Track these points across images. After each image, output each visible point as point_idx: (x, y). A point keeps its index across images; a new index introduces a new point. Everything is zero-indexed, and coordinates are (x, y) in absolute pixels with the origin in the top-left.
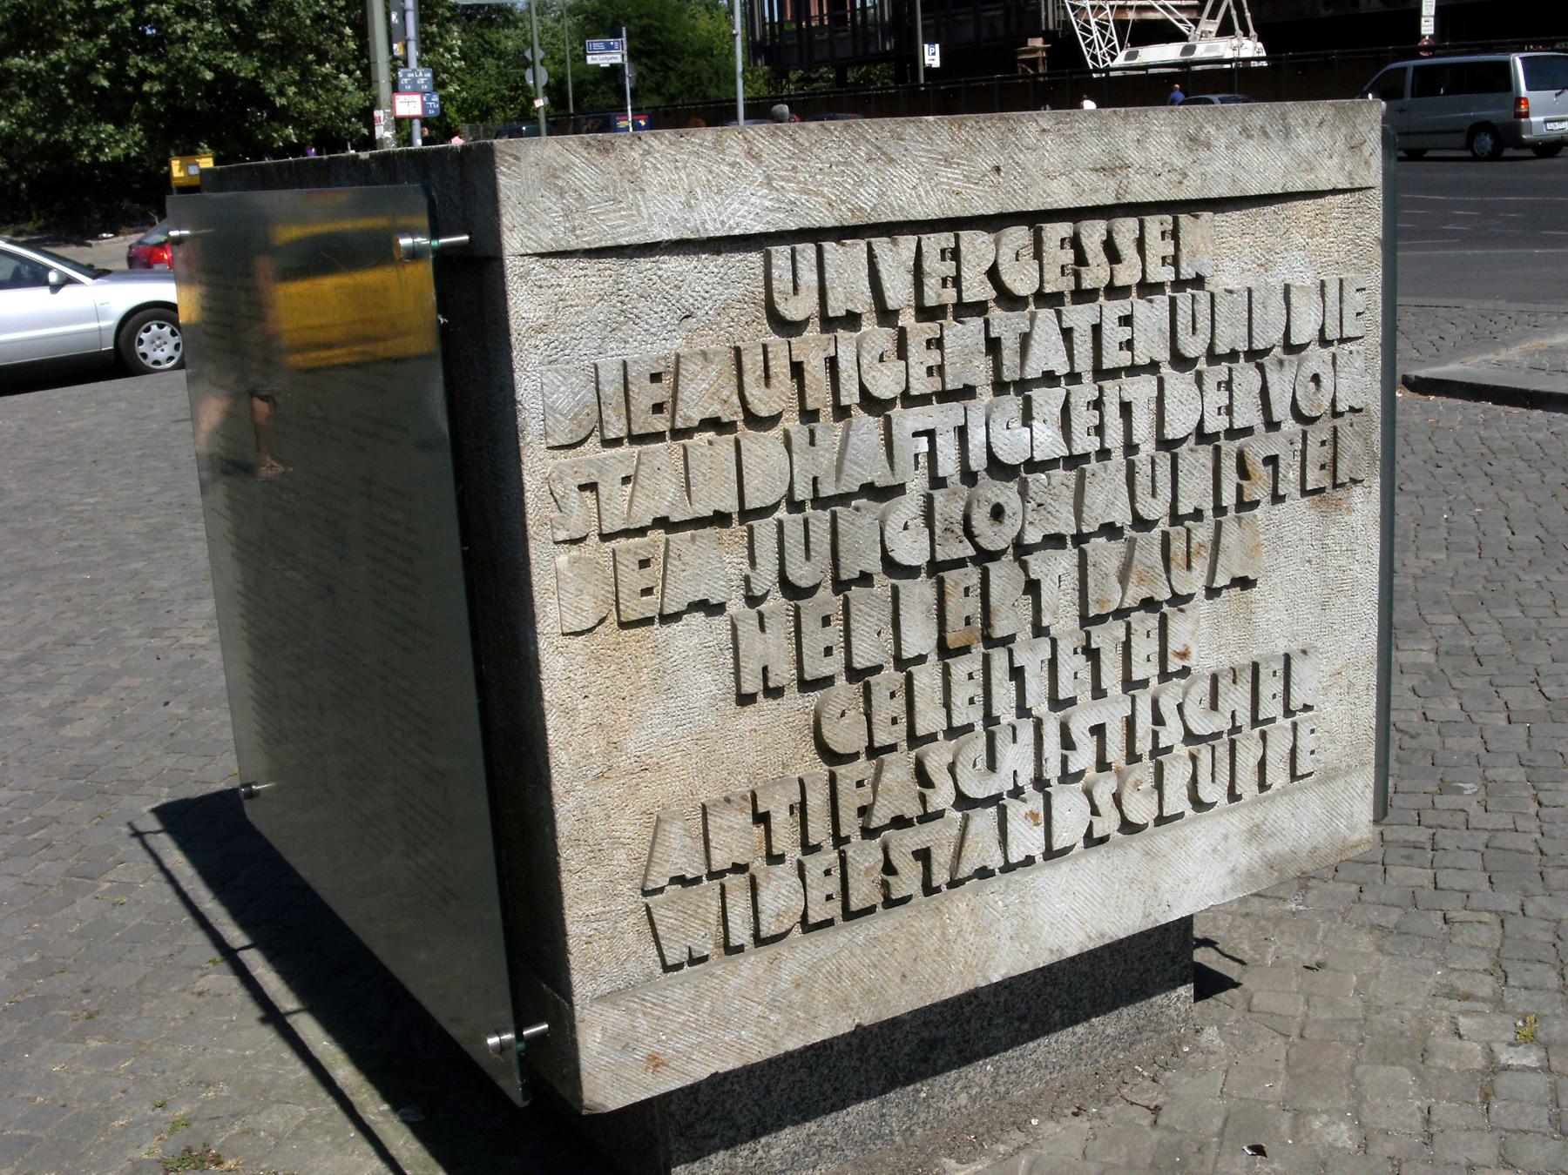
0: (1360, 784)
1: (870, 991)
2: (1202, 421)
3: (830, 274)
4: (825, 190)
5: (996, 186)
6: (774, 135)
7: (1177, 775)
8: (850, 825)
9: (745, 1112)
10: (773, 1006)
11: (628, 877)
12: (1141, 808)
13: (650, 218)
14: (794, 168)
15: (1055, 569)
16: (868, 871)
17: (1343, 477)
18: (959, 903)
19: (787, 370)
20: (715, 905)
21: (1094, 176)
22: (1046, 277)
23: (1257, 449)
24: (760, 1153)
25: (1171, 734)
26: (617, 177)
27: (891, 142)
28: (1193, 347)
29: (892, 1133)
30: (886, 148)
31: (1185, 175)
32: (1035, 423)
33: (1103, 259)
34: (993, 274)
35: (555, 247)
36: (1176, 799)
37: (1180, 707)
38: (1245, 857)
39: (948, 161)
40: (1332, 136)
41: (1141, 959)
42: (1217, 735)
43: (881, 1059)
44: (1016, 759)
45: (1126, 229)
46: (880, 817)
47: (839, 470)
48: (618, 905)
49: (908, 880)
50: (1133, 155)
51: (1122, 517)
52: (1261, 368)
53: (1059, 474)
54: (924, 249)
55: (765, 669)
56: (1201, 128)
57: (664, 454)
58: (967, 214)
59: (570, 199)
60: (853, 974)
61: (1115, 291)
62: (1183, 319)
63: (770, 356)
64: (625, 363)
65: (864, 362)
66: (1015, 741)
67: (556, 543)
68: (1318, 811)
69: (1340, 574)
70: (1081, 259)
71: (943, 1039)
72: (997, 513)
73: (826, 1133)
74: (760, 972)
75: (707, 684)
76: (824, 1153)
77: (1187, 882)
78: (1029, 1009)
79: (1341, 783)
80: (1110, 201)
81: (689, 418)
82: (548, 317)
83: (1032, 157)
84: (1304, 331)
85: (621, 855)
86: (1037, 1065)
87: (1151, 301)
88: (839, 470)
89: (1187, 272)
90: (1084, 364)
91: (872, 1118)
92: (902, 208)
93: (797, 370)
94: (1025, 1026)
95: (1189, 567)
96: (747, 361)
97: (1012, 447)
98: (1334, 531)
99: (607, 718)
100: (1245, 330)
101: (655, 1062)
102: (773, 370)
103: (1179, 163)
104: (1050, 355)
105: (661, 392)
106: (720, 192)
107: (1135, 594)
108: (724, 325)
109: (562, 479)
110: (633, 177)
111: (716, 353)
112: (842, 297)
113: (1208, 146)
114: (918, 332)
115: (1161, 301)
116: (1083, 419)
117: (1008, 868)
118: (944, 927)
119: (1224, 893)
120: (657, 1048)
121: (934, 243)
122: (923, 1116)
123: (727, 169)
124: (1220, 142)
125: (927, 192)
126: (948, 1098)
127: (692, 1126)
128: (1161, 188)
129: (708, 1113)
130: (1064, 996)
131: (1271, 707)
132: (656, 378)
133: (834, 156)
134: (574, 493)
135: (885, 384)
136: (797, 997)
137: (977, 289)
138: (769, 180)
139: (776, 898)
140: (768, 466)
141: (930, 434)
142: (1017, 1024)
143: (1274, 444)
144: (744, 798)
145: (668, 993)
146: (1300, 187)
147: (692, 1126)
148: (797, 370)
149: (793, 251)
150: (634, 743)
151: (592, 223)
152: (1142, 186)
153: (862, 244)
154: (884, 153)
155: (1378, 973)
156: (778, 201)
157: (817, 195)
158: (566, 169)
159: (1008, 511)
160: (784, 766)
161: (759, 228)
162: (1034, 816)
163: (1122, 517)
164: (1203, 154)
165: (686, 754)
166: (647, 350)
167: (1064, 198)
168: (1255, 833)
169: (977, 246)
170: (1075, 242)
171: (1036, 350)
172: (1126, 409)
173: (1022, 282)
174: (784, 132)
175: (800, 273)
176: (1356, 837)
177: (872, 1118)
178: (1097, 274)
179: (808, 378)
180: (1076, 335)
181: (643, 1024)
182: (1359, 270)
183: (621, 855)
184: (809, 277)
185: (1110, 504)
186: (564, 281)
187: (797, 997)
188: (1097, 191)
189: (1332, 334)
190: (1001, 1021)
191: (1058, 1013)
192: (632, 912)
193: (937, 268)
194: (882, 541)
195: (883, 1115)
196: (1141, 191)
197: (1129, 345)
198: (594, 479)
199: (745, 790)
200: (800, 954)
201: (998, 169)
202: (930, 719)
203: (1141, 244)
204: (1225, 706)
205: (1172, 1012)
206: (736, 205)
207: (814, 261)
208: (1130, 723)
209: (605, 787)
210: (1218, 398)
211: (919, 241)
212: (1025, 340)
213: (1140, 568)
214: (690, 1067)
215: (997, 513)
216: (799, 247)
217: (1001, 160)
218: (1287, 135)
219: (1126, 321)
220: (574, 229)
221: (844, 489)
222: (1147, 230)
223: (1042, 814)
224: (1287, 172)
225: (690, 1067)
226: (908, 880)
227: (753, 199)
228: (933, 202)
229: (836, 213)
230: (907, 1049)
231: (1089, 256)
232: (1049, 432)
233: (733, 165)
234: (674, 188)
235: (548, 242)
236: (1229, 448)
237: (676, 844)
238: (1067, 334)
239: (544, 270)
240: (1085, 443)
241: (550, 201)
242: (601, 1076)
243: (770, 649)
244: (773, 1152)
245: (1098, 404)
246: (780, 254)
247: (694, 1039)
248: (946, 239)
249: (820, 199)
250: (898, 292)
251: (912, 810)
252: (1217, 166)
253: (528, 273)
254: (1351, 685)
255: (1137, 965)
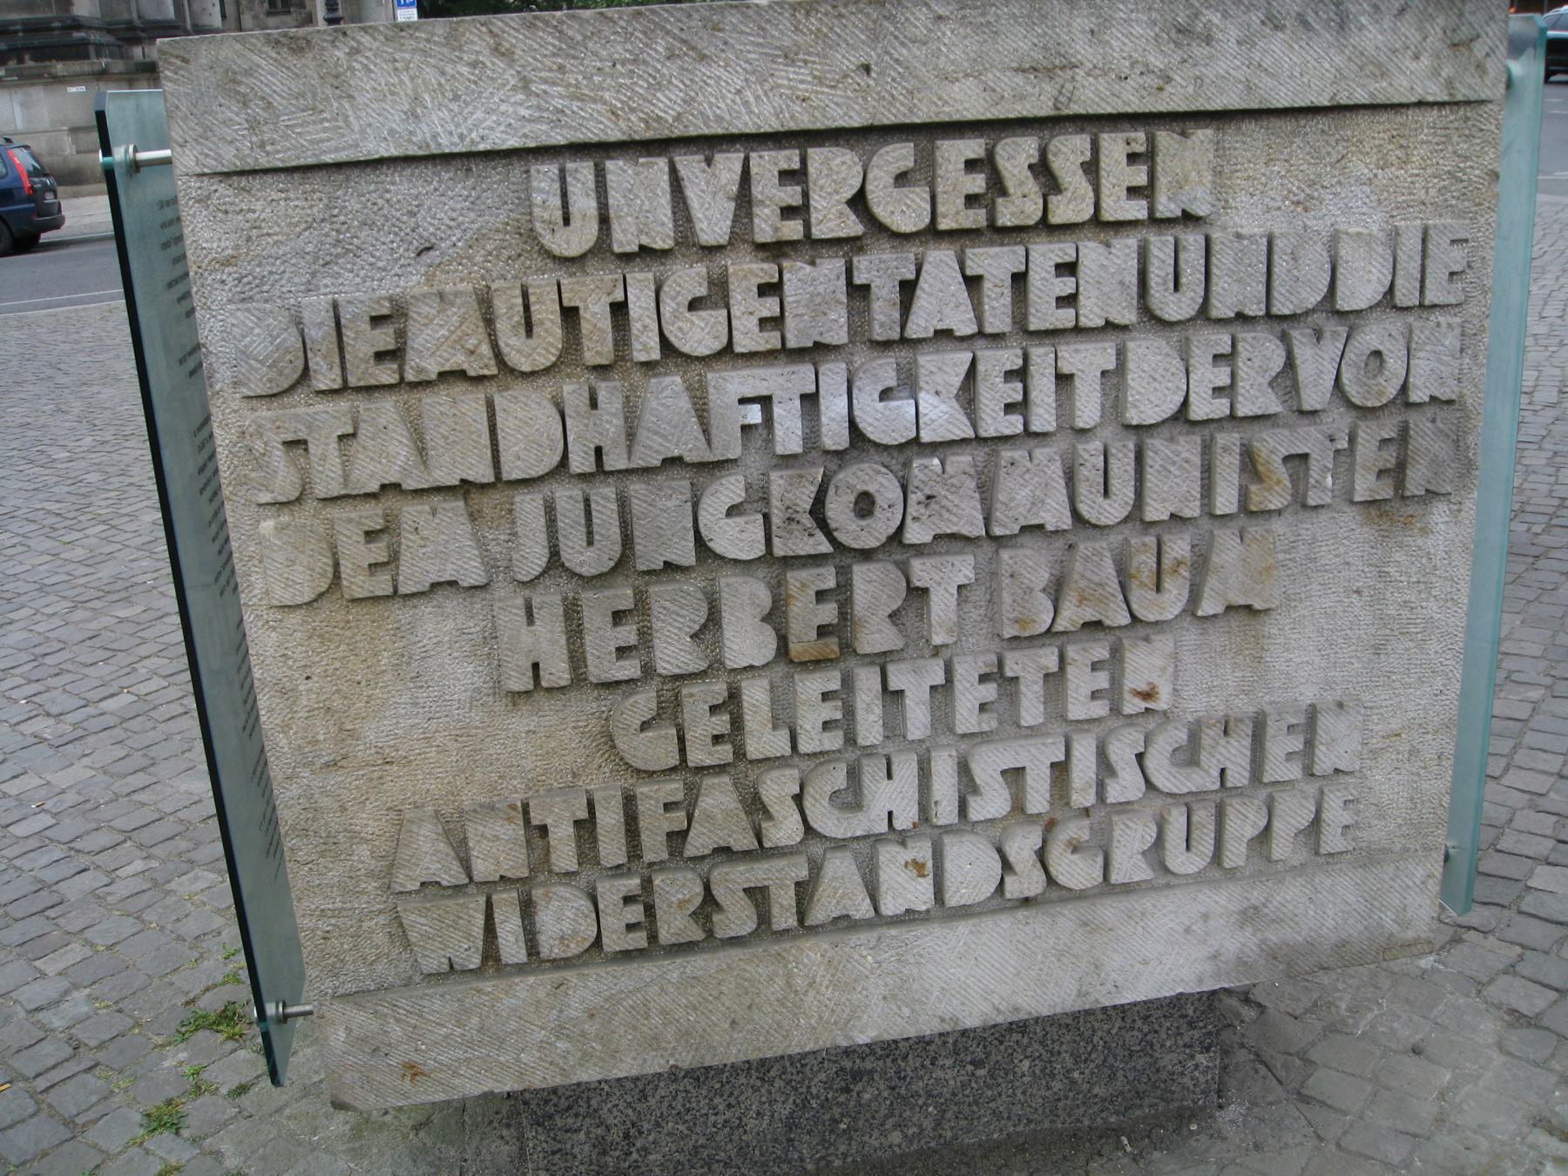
0: (1420, 873)
1: (688, 1033)
2: (1185, 403)
3: (615, 198)
4: (607, 95)
5: (864, 92)
6: (531, 26)
7: (1131, 840)
8: (654, 847)
9: (616, 1113)
10: (560, 1031)
11: (370, 874)
12: (1076, 871)
13: (363, 131)
14: (561, 68)
15: (945, 578)
16: (682, 904)
17: (1414, 486)
18: (812, 954)
19: (557, 317)
20: (480, 919)
21: (1019, 79)
22: (941, 209)
23: (1273, 446)
24: (635, 1156)
25: (1126, 786)
26: (316, 82)
27: (704, 34)
28: (1175, 307)
29: (802, 1160)
30: (695, 40)
31: (1169, 80)
32: (922, 395)
33: (1032, 186)
34: (859, 202)
35: (239, 165)
36: (1129, 864)
37: (1140, 757)
38: (1235, 942)
39: (789, 58)
40: (1420, 29)
41: (1146, 1018)
42: (1199, 795)
43: (789, 1082)
44: (891, 797)
45: (1069, 151)
46: (699, 843)
47: (631, 436)
48: (361, 904)
49: (737, 917)
50: (1082, 50)
51: (1055, 515)
52: (1285, 338)
53: (961, 461)
54: (754, 170)
55: (536, 666)
56: (1197, 15)
57: (387, 409)
58: (819, 126)
59: (256, 108)
60: (664, 1012)
61: (1046, 227)
62: (1160, 272)
63: (532, 299)
64: (335, 306)
65: (666, 310)
66: (890, 776)
67: (260, 505)
68: (1351, 899)
69: (1405, 613)
70: (997, 185)
71: (871, 1072)
72: (865, 505)
73: (718, 1148)
74: (541, 994)
75: (460, 676)
76: (715, 1166)
77: (1145, 962)
78: (988, 1055)
79: (1390, 869)
80: (1045, 110)
81: (421, 370)
82: (237, 247)
83: (920, 52)
84: (1359, 291)
85: (363, 851)
86: (997, 1115)
87: (1108, 245)
88: (631, 436)
89: (1167, 207)
90: (998, 317)
91: (776, 1140)
92: (719, 119)
93: (570, 315)
94: (981, 1072)
95: (1159, 588)
96: (500, 306)
97: (887, 421)
98: (1398, 556)
99: (337, 702)
100: (1262, 288)
101: (413, 1071)
102: (535, 317)
103: (1157, 61)
104: (947, 310)
105: (384, 338)
106: (456, 98)
107: (1072, 615)
108: (479, 259)
109: (261, 435)
110: (338, 81)
111: (457, 294)
112: (633, 229)
113: (1208, 40)
114: (747, 271)
115: (1126, 245)
116: (995, 393)
117: (879, 920)
118: (789, 976)
119: (1200, 981)
120: (414, 1057)
121: (767, 163)
122: (842, 1148)
123: (465, 70)
124: (1229, 35)
125: (757, 98)
126: (876, 1134)
127: (551, 1117)
128: (1126, 96)
129: (569, 1108)
130: (1036, 1046)
131: (1279, 768)
132: (377, 321)
133: (619, 51)
134: (278, 453)
135: (700, 334)
136: (591, 1028)
137: (831, 218)
138: (525, 84)
139: (559, 920)
140: (529, 427)
141: (765, 401)
142: (970, 1068)
143: (1307, 439)
144: (513, 807)
145: (426, 1003)
146: (1361, 97)
147: (551, 1117)
148: (570, 315)
149: (562, 171)
150: (372, 733)
151: (286, 137)
152: (1097, 93)
153: (662, 163)
154: (693, 48)
155: (1478, 1078)
156: (539, 108)
157: (594, 101)
158: (249, 72)
159: (881, 501)
160: (574, 775)
161: (513, 142)
162: (919, 867)
163: (1055, 515)
164: (1199, 51)
165: (442, 750)
166: (362, 290)
167: (968, 103)
168: (1250, 916)
169: (834, 171)
170: (1042, 169)
171: (924, 301)
172: (1064, 380)
173: (903, 210)
174: (547, 23)
175: (572, 199)
176: (1410, 934)
177: (776, 1140)
178: (1021, 205)
179: (585, 327)
180: (987, 285)
181: (396, 1031)
182: (1461, 214)
183: (363, 851)
184: (584, 203)
185: (1037, 503)
186: (258, 206)
187: (591, 1028)
188: (1022, 98)
189: (1406, 294)
190: (948, 1062)
191: (1026, 1063)
192: (380, 912)
193: (771, 193)
194: (697, 532)
195: (790, 1140)
196: (1092, 97)
197: (1069, 300)
198: (302, 436)
199: (517, 799)
200: (589, 988)
201: (867, 69)
202: (763, 740)
203: (1092, 168)
204: (1211, 762)
205: (1187, 1081)
206: (479, 114)
207: (591, 184)
208: (1061, 770)
209: (336, 778)
210: (1208, 376)
211: (747, 160)
212: (908, 289)
213: (1083, 584)
214: (457, 1082)
215: (865, 505)
216: (570, 165)
217: (873, 57)
218: (1342, 26)
219: (1068, 269)
220: (262, 145)
221: (638, 462)
222: (1104, 152)
223: (930, 864)
224: (1340, 76)
225: (457, 1082)
226: (737, 917)
227: (503, 107)
228: (767, 109)
229: (622, 124)
230: (822, 1076)
231: (1011, 185)
232: (944, 408)
233: (474, 65)
234: (393, 93)
235: (230, 158)
236: (1229, 440)
237: (426, 847)
238: (973, 283)
239: (230, 192)
240: (995, 422)
241: (230, 110)
242: (348, 1075)
243: (546, 641)
244: (651, 1157)
245: (1021, 374)
246: (544, 175)
247: (460, 1054)
248: (788, 158)
249: (599, 107)
250: (713, 222)
251: (743, 840)
252: (1222, 67)
253: (208, 197)
254: (1413, 752)
255: (1139, 1023)
